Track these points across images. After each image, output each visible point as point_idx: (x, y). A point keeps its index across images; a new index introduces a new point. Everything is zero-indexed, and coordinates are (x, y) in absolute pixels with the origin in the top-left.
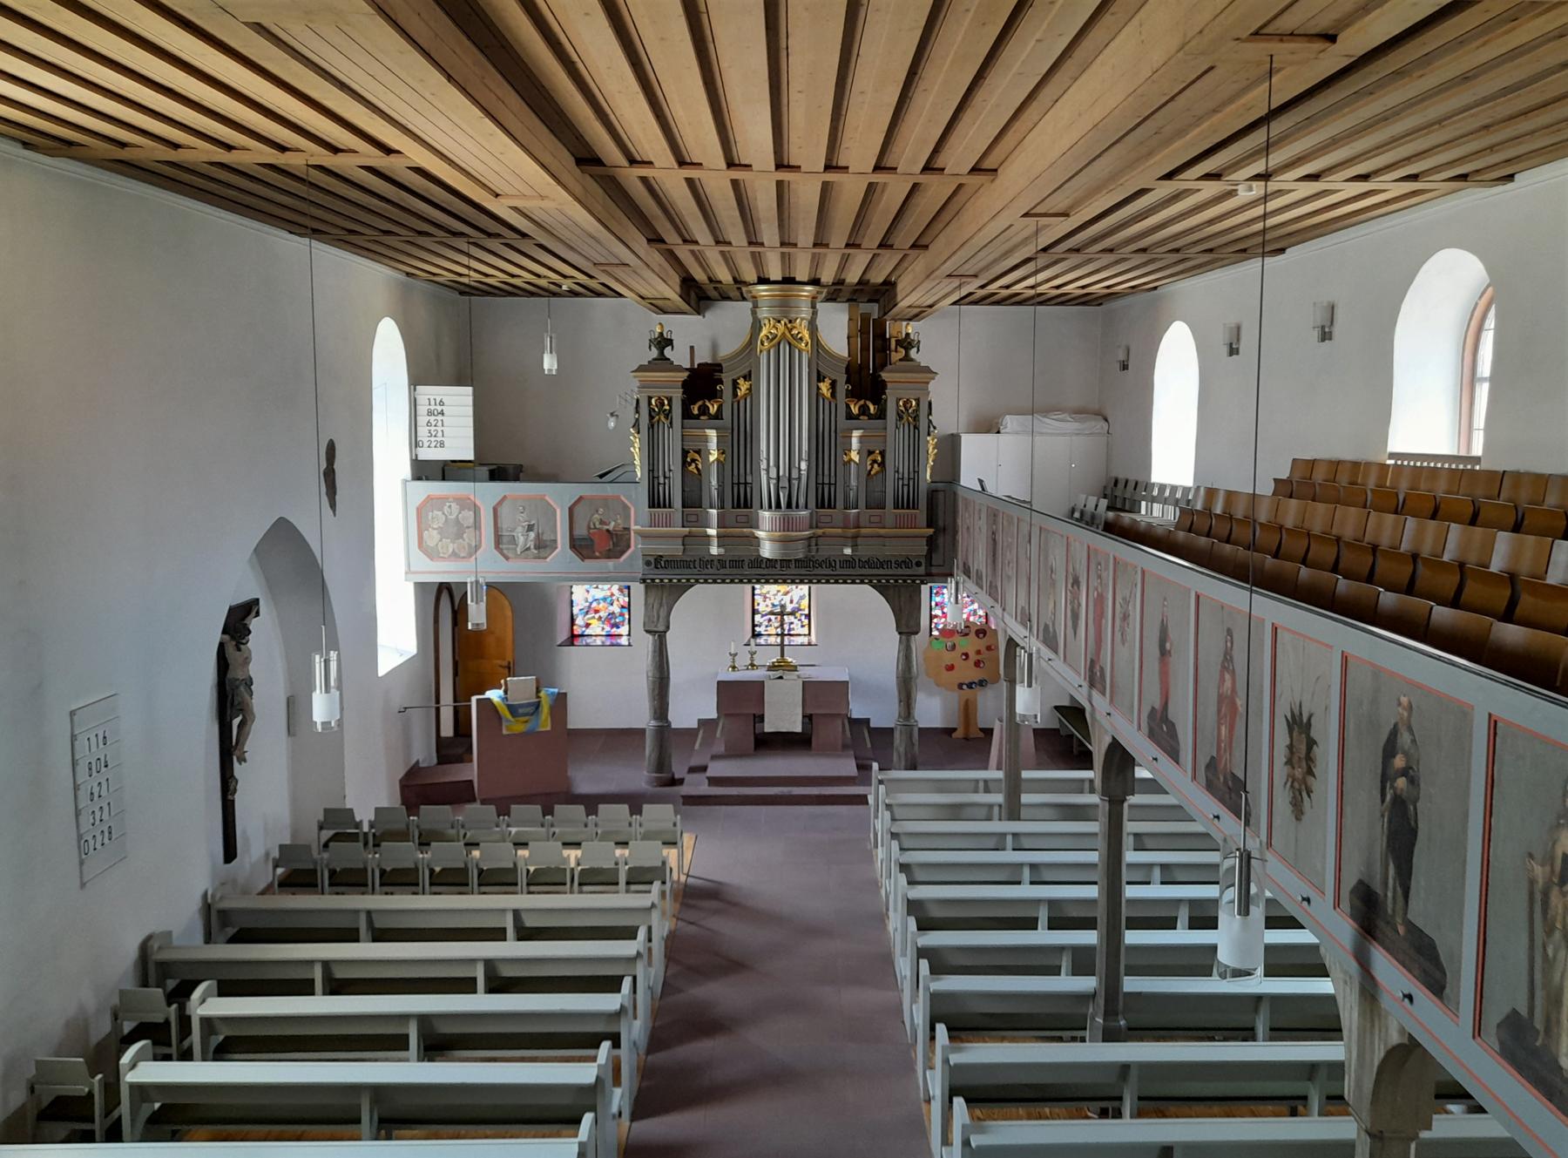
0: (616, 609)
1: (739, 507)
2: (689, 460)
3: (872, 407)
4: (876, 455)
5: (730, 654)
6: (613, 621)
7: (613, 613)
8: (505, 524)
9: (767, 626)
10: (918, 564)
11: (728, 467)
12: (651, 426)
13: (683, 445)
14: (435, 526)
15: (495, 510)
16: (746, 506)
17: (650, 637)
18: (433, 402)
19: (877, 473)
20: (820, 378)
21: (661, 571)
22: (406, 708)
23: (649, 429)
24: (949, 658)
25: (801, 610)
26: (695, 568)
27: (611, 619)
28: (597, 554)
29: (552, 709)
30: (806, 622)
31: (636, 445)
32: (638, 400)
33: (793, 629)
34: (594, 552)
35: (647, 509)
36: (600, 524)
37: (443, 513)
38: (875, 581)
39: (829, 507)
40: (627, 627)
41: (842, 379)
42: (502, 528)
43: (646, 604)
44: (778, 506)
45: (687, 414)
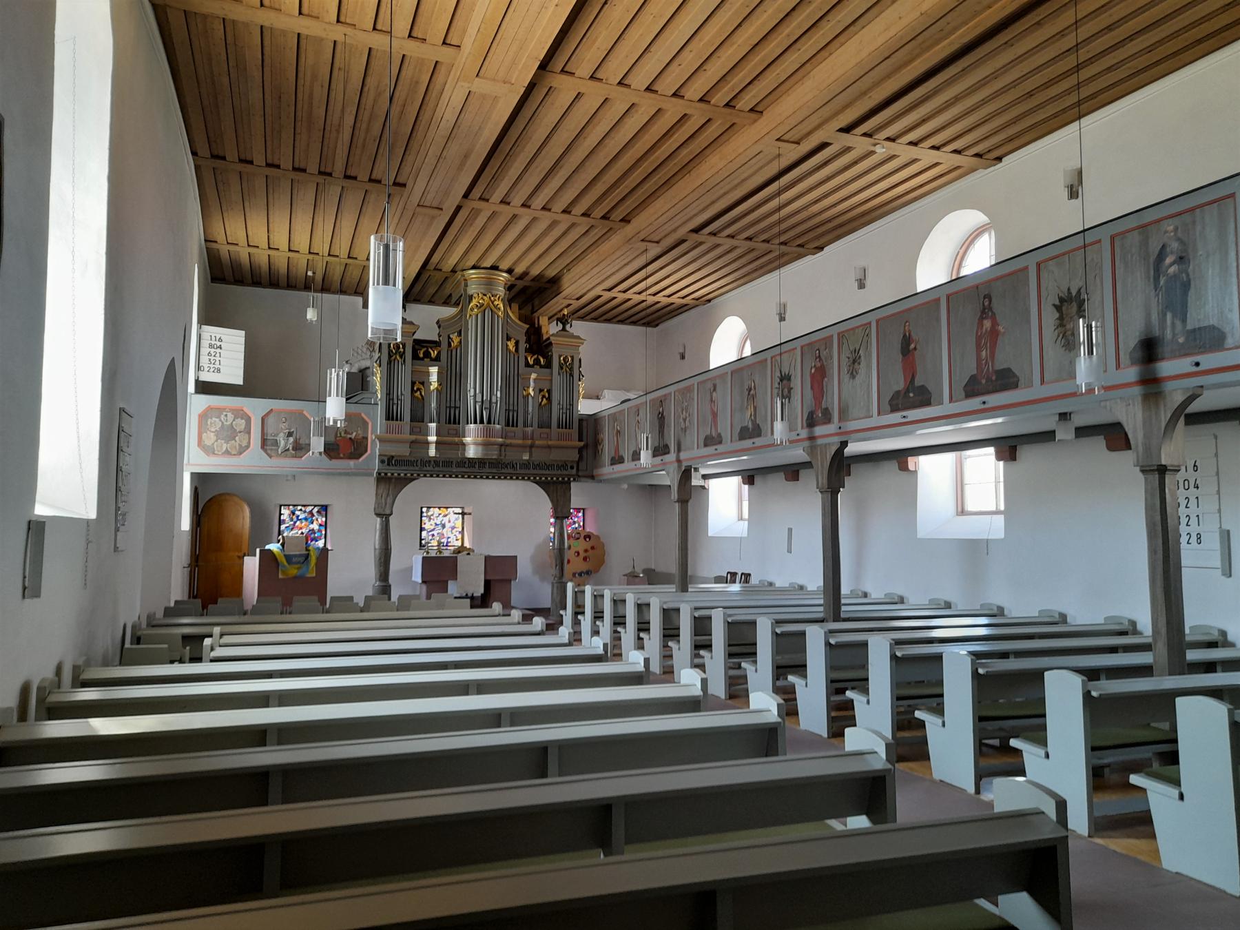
1: (450, 423)
2: (415, 389)
3: (542, 360)
4: (546, 394)
7: (313, 530)
8: (270, 430)
10: (572, 468)
11: (444, 395)
12: (389, 363)
15: (263, 419)
16: (455, 423)
17: (379, 519)
18: (213, 338)
19: (545, 405)
20: (509, 339)
21: (391, 467)
30: (459, 537)
33: (450, 542)
36: (345, 433)
37: (221, 420)
39: (513, 426)
40: (323, 541)
41: (523, 339)
43: (376, 494)
44: (482, 422)
45: (415, 357)
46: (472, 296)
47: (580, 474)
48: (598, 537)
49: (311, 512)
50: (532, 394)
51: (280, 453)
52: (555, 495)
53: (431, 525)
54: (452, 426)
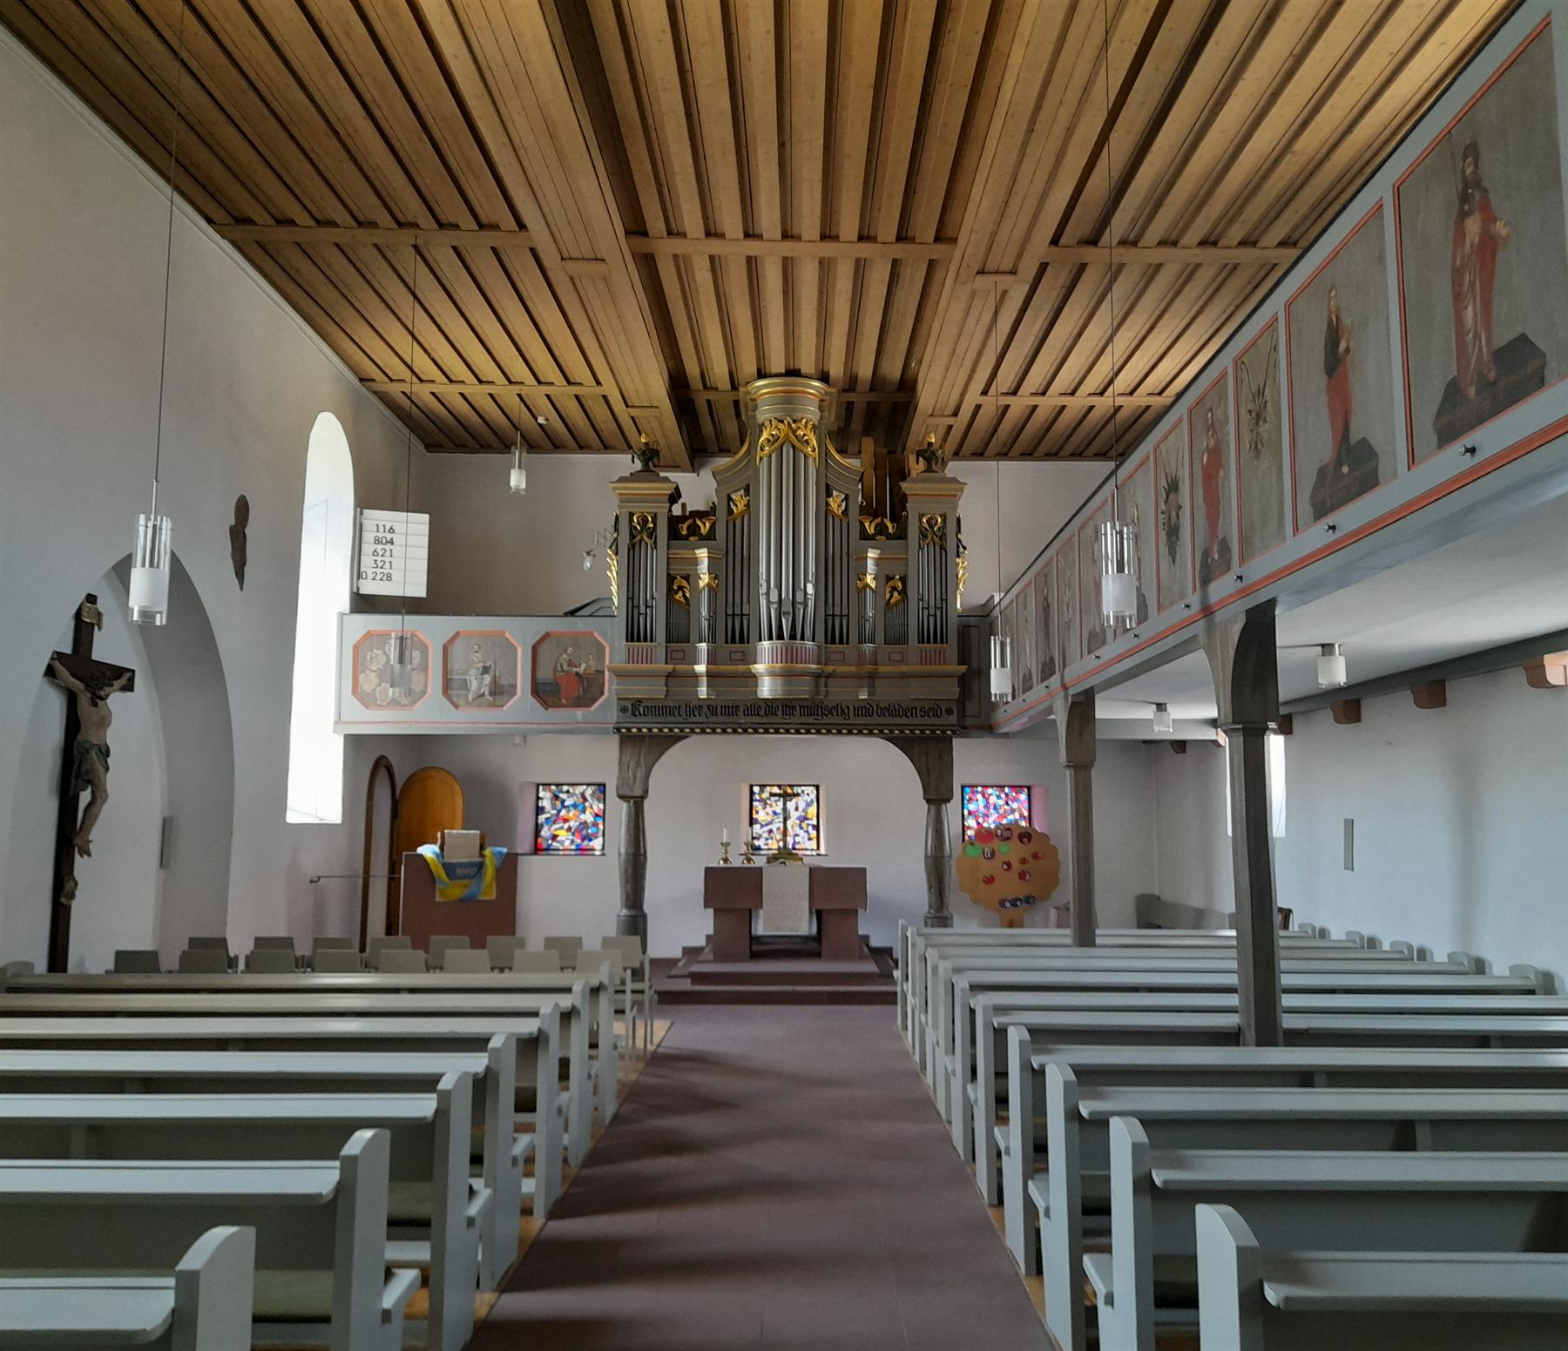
0: (588, 817)
1: (733, 641)
2: (675, 587)
3: (889, 525)
5: (722, 844)
6: (584, 832)
7: (586, 822)
8: (456, 664)
9: (767, 839)
10: (950, 712)
12: (632, 547)
13: (668, 569)
14: (374, 668)
16: (742, 641)
17: (625, 805)
18: (381, 529)
19: (897, 602)
21: (638, 719)
22: (319, 878)
23: (629, 550)
24: (987, 868)
25: (806, 819)
26: (680, 715)
27: (582, 829)
28: (564, 701)
29: (499, 872)
30: (814, 833)
31: (613, 568)
32: (617, 517)
34: (560, 699)
35: (625, 643)
36: (569, 665)
37: (385, 653)
38: (896, 732)
39: (841, 642)
42: (452, 671)
43: (620, 764)
44: (780, 637)
45: (674, 534)
46: (763, 424)
47: (969, 722)
48: (1044, 837)
49: (583, 795)
50: (873, 585)
51: (470, 700)
52: (924, 759)
53: (768, 814)
54: (738, 646)
